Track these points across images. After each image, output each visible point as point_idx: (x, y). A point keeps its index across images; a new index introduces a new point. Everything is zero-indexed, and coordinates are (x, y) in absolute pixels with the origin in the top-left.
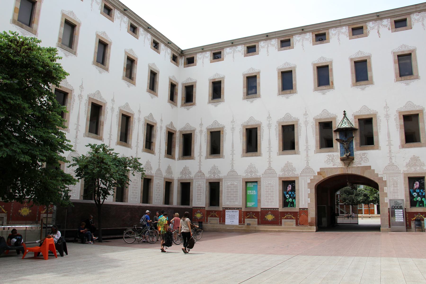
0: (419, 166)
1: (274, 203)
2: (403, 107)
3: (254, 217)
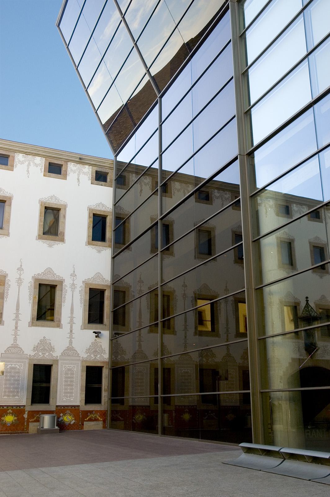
1: (73, 398)
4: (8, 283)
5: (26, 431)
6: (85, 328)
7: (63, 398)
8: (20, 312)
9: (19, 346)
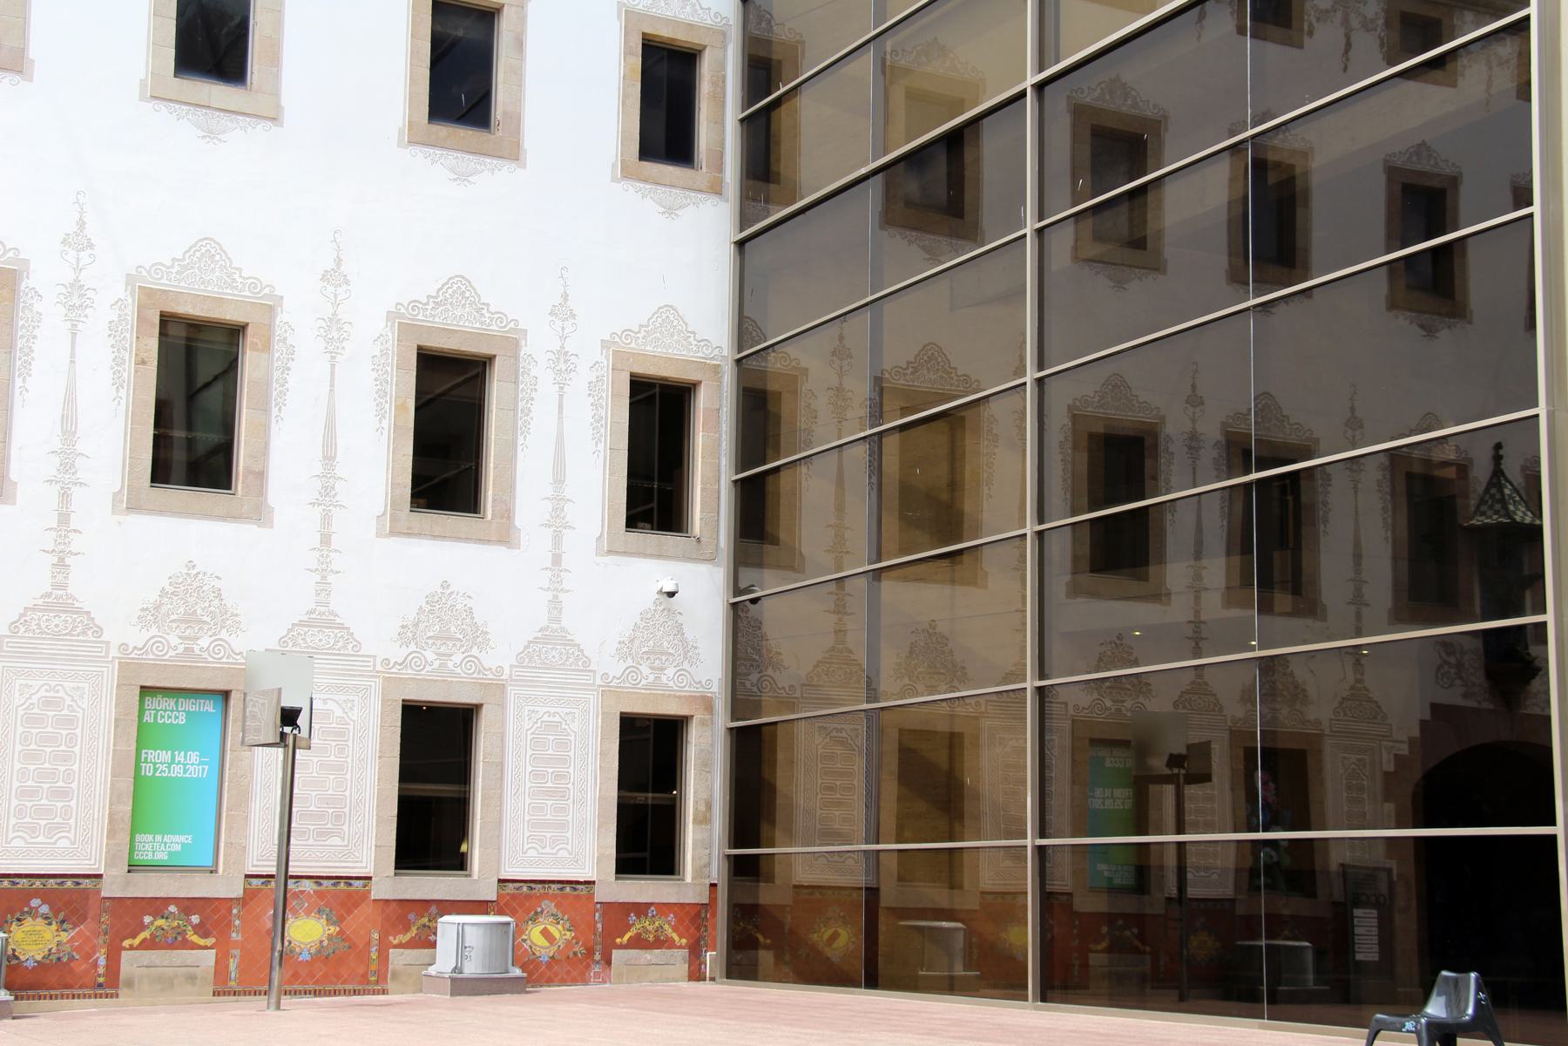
0: (1131, 695)
1: (569, 847)
2: (425, 301)
3: (195, 939)
4: (285, 339)
5: (377, 982)
6: (134, 507)
7: (526, 847)
8: (79, 447)
9: (338, 621)
